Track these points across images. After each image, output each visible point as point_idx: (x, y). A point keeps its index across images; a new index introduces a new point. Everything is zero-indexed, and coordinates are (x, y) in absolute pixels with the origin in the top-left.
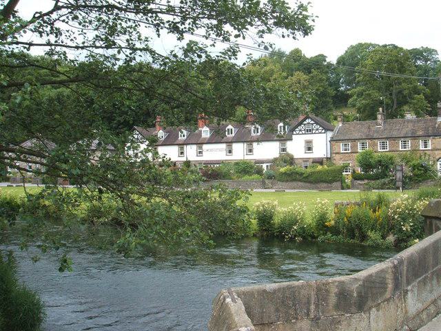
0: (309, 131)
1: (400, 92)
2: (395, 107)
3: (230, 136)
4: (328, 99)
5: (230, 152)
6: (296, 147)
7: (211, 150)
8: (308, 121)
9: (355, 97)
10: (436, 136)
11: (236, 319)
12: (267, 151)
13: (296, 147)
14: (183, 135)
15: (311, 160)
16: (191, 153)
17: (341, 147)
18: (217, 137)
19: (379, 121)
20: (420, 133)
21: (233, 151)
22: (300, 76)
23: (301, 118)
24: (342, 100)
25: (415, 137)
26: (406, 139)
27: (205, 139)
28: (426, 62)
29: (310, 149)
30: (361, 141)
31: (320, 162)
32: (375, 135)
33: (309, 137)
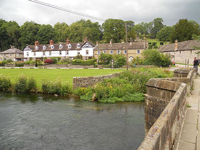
0: (87, 47)
1: (120, 34)
2: (118, 40)
3: (44, 49)
4: (98, 36)
5: (61, 54)
6: (83, 52)
7: (56, 53)
8: (87, 43)
9: (105, 36)
10: (129, 49)
11: (145, 144)
12: (73, 54)
13: (83, 52)
14: (44, 47)
15: (88, 57)
16: (64, 53)
17: (97, 52)
18: (65, 49)
19: (111, 44)
20: (124, 48)
21: (69, 53)
22: (88, 28)
23: (85, 42)
24: (101, 38)
25: (122, 49)
26: (119, 50)
27: (52, 49)
28: (131, 26)
29: (87, 53)
30: (104, 51)
31: (90, 58)
32: (109, 49)
33: (87, 49)
